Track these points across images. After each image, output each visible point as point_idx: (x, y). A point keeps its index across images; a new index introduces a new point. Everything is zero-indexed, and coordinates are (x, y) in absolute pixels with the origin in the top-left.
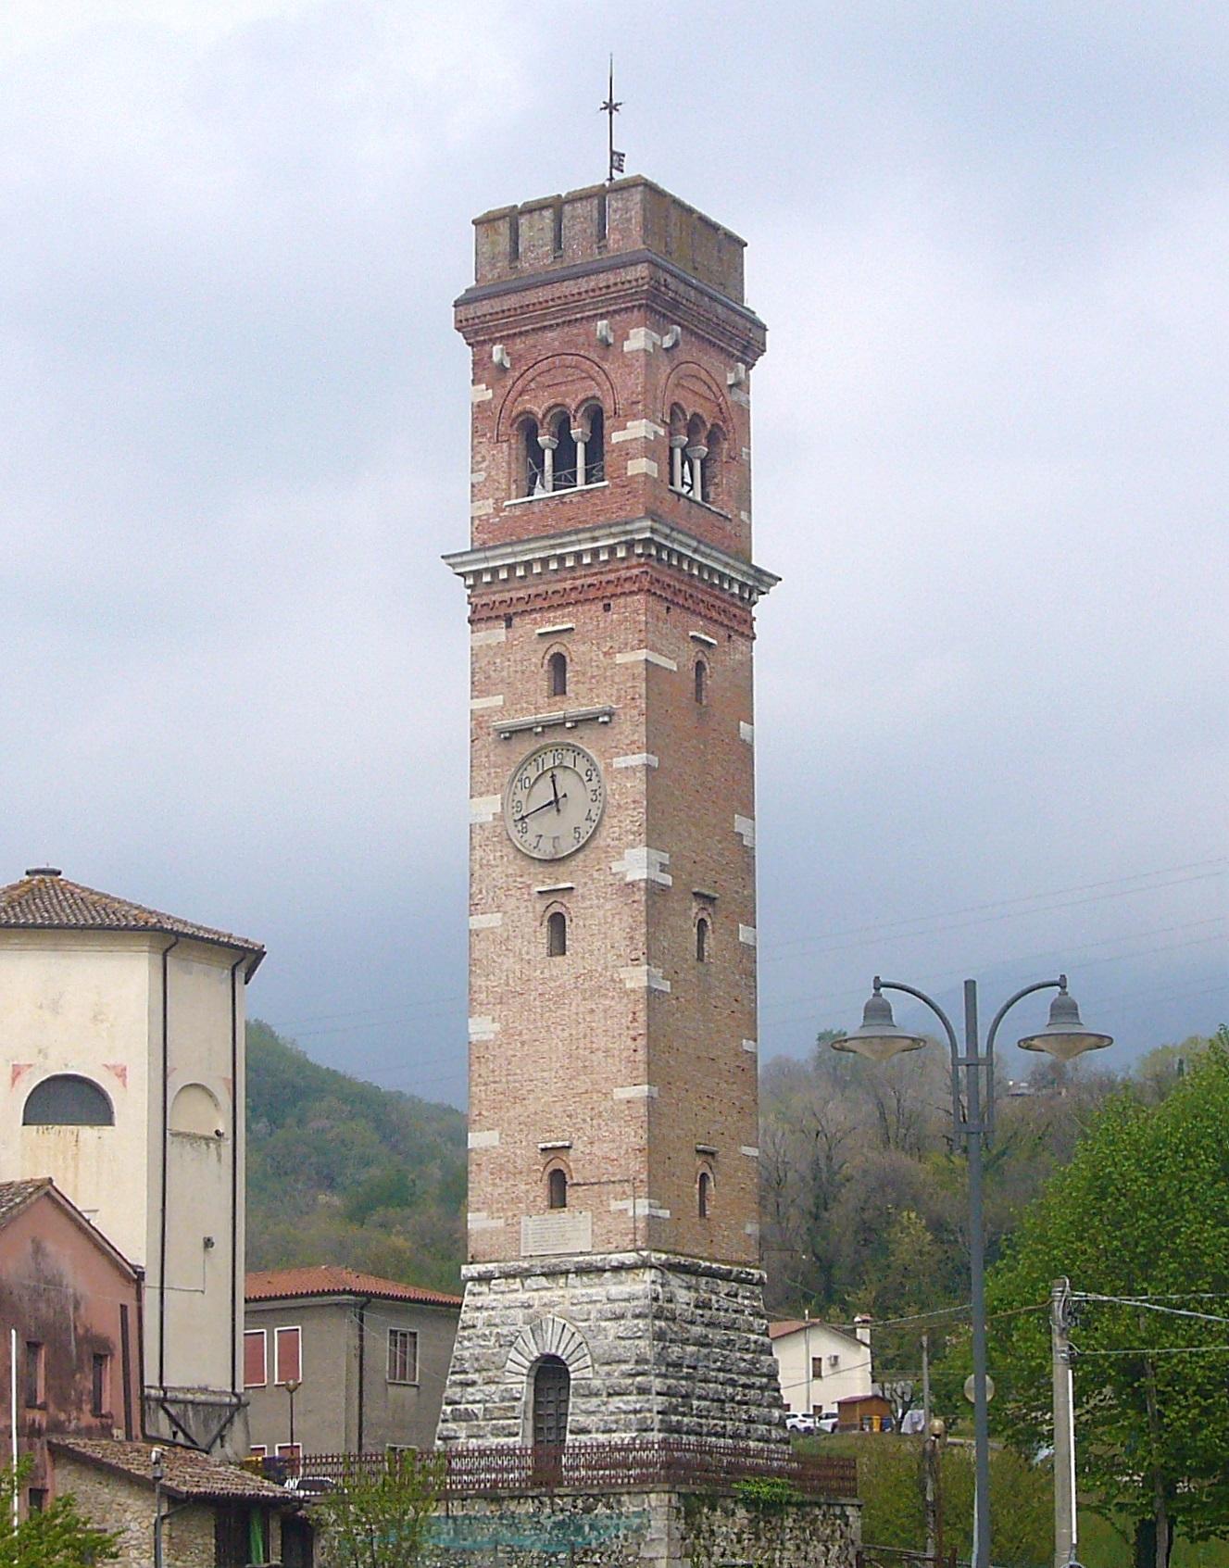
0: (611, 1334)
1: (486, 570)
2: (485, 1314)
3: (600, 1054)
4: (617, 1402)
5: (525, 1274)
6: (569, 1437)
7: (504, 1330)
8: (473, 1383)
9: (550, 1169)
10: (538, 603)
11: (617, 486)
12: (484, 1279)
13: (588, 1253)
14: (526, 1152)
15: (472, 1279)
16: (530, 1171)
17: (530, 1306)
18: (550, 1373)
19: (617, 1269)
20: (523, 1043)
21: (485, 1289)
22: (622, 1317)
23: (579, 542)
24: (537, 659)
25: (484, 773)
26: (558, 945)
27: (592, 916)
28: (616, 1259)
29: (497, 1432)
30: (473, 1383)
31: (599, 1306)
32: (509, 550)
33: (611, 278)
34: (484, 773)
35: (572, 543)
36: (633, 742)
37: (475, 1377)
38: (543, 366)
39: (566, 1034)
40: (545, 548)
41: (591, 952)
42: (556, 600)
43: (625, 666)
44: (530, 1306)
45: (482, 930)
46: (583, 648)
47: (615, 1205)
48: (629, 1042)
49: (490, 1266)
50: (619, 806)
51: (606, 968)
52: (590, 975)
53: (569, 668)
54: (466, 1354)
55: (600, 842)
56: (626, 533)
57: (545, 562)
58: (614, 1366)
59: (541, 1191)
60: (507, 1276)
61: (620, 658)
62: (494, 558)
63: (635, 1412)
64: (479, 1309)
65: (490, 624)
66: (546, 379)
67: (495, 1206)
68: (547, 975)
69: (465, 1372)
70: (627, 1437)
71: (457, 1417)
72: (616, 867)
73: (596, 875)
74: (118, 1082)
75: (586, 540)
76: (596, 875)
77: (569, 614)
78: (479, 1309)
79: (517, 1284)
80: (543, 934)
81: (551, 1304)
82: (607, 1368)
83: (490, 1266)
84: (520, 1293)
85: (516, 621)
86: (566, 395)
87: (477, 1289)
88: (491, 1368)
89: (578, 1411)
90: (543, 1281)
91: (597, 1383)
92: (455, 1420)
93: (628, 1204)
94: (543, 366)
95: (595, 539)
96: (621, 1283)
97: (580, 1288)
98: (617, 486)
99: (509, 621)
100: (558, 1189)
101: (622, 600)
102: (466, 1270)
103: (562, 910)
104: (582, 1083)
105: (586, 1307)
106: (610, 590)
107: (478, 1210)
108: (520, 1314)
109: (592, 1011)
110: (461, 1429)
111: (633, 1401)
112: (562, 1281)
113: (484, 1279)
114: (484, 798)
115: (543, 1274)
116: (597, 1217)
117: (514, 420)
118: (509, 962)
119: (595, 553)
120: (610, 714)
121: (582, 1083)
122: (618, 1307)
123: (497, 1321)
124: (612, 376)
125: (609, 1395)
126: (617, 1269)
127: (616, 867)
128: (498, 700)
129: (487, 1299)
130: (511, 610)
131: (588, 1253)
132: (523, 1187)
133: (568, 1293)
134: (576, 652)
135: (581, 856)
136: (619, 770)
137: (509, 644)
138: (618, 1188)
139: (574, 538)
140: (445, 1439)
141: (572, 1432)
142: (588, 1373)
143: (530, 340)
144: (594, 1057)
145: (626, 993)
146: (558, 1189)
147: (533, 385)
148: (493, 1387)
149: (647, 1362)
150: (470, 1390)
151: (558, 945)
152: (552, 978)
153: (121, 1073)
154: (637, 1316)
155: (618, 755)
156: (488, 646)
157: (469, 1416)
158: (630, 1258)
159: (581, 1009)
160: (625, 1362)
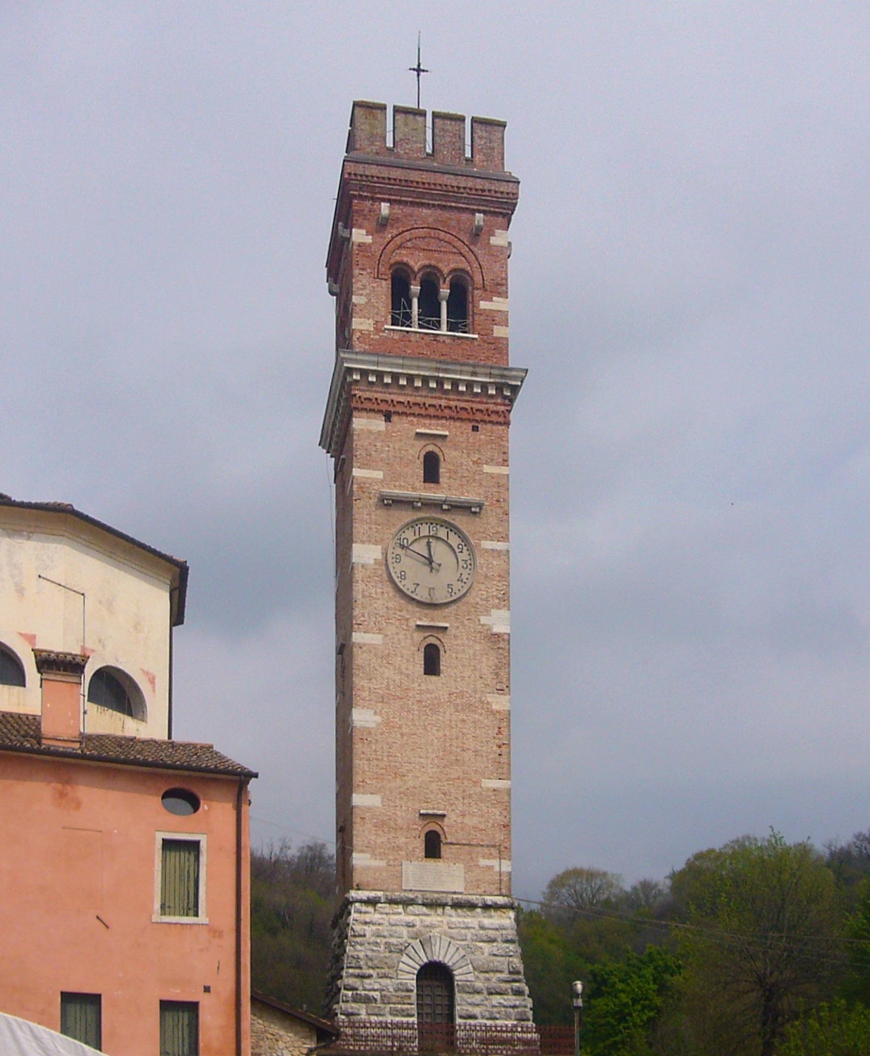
0: (486, 951)
1: (374, 372)
2: (374, 928)
3: (471, 753)
4: (496, 999)
5: (407, 903)
6: (458, 1021)
7: (393, 940)
8: (370, 976)
9: (427, 829)
10: (416, 410)
11: (485, 341)
12: (372, 902)
13: (461, 893)
14: (406, 813)
15: (361, 901)
16: (409, 829)
17: (414, 926)
18: (436, 976)
19: (486, 907)
20: (402, 735)
21: (370, 909)
22: (494, 941)
23: (461, 373)
24: (417, 450)
25: (366, 527)
26: (432, 665)
27: (463, 651)
28: (489, 899)
29: (394, 1013)
30: (370, 976)
31: (472, 930)
32: (401, 361)
33: (487, 185)
34: (366, 527)
35: (455, 372)
36: (497, 533)
37: (371, 972)
38: (421, 233)
39: (441, 734)
40: (430, 369)
41: (463, 678)
42: (432, 411)
43: (492, 476)
44: (414, 926)
45: (365, 645)
46: (455, 453)
47: (483, 862)
48: (495, 748)
49: (380, 894)
50: (486, 576)
51: (475, 692)
52: (461, 694)
53: (442, 464)
54: (361, 955)
55: (470, 599)
56: (502, 376)
57: (425, 380)
58: (492, 974)
59: (419, 845)
60: (392, 902)
61: (487, 469)
62: (385, 364)
63: (514, 1007)
64: (366, 923)
65: (372, 415)
66: (421, 244)
67: (377, 851)
68: (423, 687)
69: (360, 968)
70: (510, 1023)
71: (356, 999)
72: (484, 620)
73: (466, 622)
74: (149, 687)
75: (467, 373)
76: (466, 622)
77: (442, 426)
78: (366, 923)
79: (400, 908)
80: (420, 658)
81: (432, 926)
82: (487, 975)
83: (380, 894)
84: (401, 915)
85: (395, 418)
86: (440, 261)
87: (364, 908)
88: (386, 970)
89: (463, 1003)
90: (424, 909)
91: (479, 985)
92: (355, 1001)
93: (494, 863)
94: (421, 233)
95: (474, 374)
96: (491, 917)
97: (455, 917)
98: (485, 341)
99: (388, 417)
100: (433, 847)
101: (489, 426)
102: (353, 894)
103: (437, 643)
104: (456, 772)
105: (463, 931)
106: (479, 416)
107: (362, 851)
108: (404, 931)
109: (463, 721)
110: (362, 1010)
111: (512, 999)
112: (440, 910)
113: (372, 902)
114: (366, 546)
115: (424, 904)
116: (468, 869)
117: (391, 266)
118: (389, 673)
119: (470, 385)
120: (480, 506)
121: (456, 772)
122: (491, 933)
123: (386, 933)
124: (480, 259)
125: (490, 994)
126: (486, 907)
127: (484, 620)
128: (379, 475)
129: (376, 917)
130: (392, 409)
131: (461, 893)
132: (403, 840)
133: (445, 919)
134: (450, 457)
135: (454, 607)
136: (487, 551)
137: (388, 434)
138: (486, 850)
139: (458, 368)
140: (348, 1015)
141: (461, 1017)
142: (470, 977)
143: (408, 210)
144: (465, 754)
145: (493, 713)
146: (433, 847)
147: (409, 244)
148: (388, 981)
149: (518, 973)
150: (367, 981)
151: (432, 665)
152: (429, 691)
153: (152, 681)
154: (507, 941)
155: (486, 539)
156: (370, 432)
157: (368, 1000)
158: (500, 900)
159: (454, 718)
160: (501, 972)
